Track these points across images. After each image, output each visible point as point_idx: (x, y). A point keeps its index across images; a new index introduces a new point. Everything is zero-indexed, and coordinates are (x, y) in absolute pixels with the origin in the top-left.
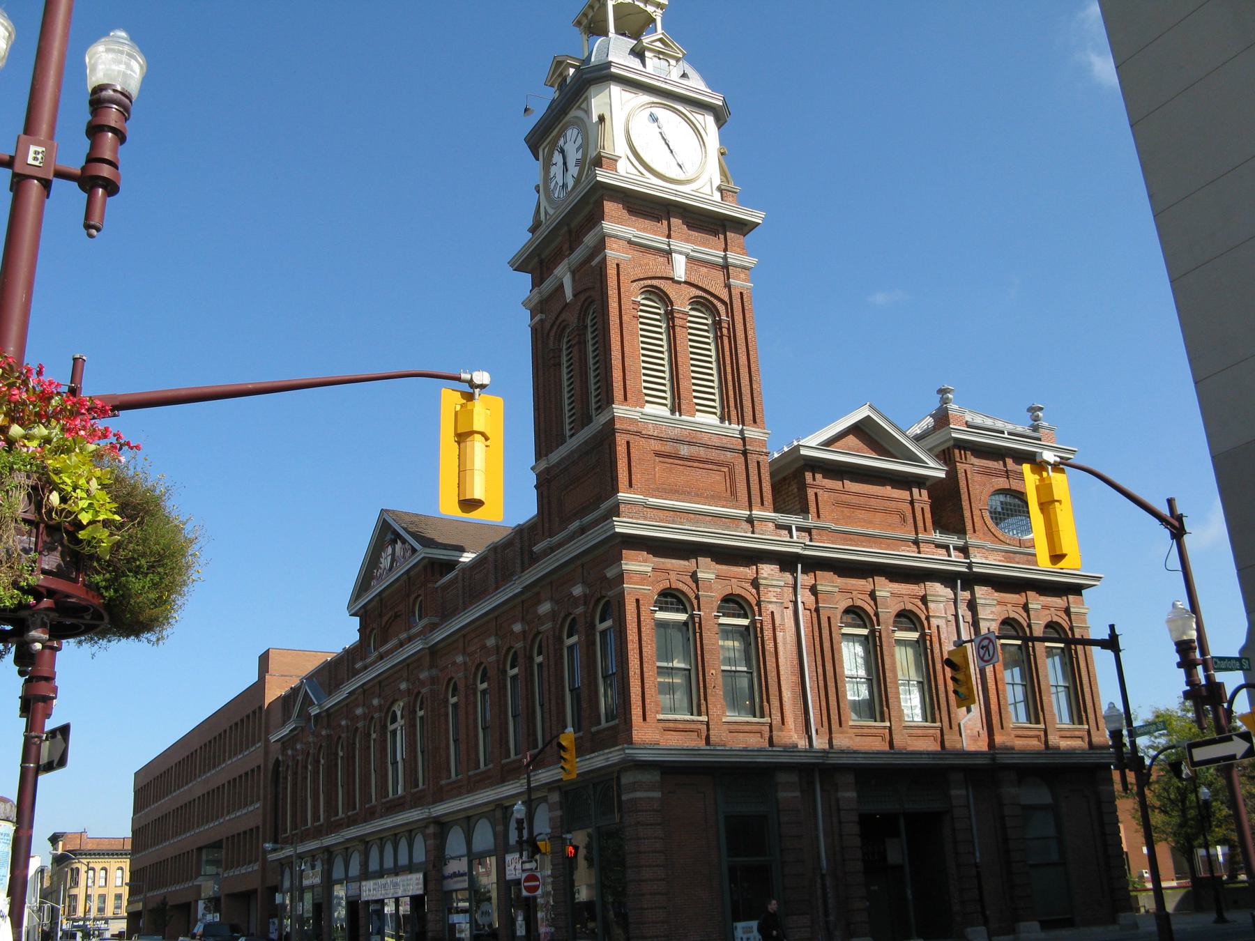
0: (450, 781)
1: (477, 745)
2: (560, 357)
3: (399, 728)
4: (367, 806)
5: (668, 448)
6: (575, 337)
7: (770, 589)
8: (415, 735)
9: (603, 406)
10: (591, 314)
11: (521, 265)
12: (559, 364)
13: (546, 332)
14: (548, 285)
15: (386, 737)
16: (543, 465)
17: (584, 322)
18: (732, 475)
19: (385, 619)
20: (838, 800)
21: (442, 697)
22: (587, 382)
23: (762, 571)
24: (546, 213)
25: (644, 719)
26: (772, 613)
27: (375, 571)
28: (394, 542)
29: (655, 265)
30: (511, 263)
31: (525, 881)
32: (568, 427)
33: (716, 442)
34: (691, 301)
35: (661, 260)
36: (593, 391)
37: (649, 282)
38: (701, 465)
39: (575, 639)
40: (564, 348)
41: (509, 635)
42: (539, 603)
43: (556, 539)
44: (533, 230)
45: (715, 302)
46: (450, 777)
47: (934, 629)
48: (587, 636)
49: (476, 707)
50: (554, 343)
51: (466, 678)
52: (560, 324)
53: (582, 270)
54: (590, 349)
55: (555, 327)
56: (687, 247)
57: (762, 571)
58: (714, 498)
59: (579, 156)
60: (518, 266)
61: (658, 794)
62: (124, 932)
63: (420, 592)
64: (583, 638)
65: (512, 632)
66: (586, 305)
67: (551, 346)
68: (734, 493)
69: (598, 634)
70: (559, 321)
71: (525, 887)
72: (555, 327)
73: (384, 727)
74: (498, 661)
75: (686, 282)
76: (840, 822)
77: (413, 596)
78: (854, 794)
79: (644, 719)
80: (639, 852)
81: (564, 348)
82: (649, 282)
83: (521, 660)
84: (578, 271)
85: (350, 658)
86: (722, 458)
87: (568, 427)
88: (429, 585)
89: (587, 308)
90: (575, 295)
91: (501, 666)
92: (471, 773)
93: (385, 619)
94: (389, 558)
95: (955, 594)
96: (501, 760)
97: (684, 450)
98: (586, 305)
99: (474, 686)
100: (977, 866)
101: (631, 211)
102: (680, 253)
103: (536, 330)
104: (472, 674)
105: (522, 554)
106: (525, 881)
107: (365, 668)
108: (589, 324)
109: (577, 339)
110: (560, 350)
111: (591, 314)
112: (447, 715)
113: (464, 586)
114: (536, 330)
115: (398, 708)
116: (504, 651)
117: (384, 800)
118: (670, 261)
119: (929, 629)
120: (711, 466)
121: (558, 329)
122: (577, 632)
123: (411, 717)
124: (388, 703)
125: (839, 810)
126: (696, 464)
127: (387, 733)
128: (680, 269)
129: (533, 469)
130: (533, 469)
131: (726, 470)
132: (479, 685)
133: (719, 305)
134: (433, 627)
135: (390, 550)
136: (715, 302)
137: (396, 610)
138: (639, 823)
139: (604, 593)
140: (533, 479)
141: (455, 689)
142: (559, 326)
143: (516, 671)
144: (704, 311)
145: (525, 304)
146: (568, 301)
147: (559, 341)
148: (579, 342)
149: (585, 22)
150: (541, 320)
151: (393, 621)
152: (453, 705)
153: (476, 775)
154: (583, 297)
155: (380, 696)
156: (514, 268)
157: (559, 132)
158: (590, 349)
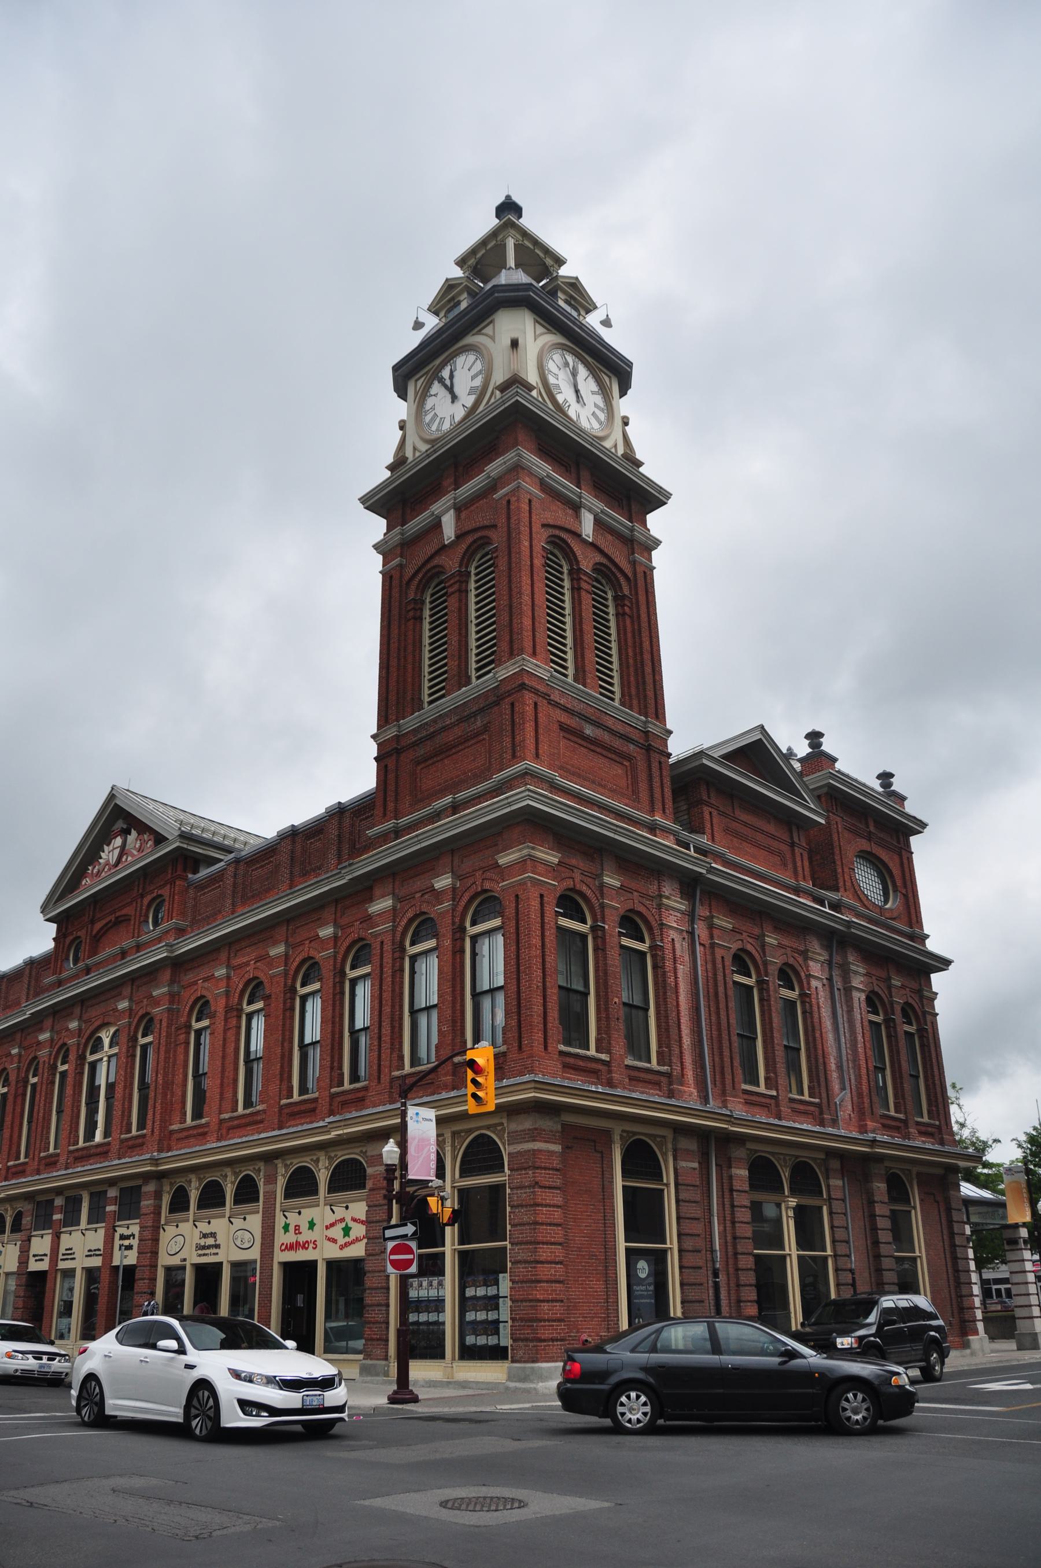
0: (235, 1114)
1: (235, 1081)
2: (421, 610)
3: (105, 1059)
4: (42, 1154)
5: (572, 722)
6: (455, 583)
7: (671, 912)
8: (133, 1068)
9: (500, 660)
10: (476, 560)
11: (376, 502)
12: (420, 619)
13: (406, 578)
14: (417, 523)
15: (83, 1069)
16: (391, 732)
17: (467, 567)
18: (634, 768)
19: (98, 926)
20: (731, 1177)
21: (183, 1020)
22: (466, 636)
23: (664, 889)
24: (415, 449)
25: (546, 1048)
26: (673, 940)
27: (90, 868)
28: (126, 832)
29: (561, 516)
30: (364, 500)
31: (392, 1253)
32: (426, 692)
33: (619, 728)
34: (598, 567)
35: (570, 512)
36: (426, 674)
37: (557, 532)
38: (604, 753)
39: (149, 1039)
40: (428, 600)
41: (308, 942)
42: (41, 1030)
43: (404, 821)
44: (391, 468)
45: (619, 575)
46: (185, 1121)
47: (813, 990)
48: (454, 940)
49: (24, 1100)
50: (416, 593)
51: (227, 994)
52: (429, 570)
54: (472, 599)
55: (420, 575)
56: (599, 505)
57: (664, 889)
58: (614, 793)
59: (478, 382)
60: (372, 504)
61: (557, 1148)
62: (255, 1261)
63: (79, 934)
64: (124, 1050)
65: (67, 1029)
66: (473, 548)
67: (411, 596)
68: (635, 792)
69: (139, 1049)
70: (429, 566)
71: (393, 1262)
72: (420, 575)
73: (82, 1058)
74: (286, 973)
75: (592, 544)
76: (733, 1206)
77: (146, 901)
78: (747, 1173)
79: (546, 1048)
80: (536, 1223)
81: (428, 600)
82: (557, 532)
83: (72, 1057)
84: (466, 508)
85: (34, 973)
86: (625, 749)
87: (426, 692)
88: (177, 883)
89: (432, 578)
90: (459, 537)
91: (290, 982)
92: (11, 1163)
93: (98, 926)
94: (117, 852)
95: (831, 956)
96: (280, 1099)
97: (589, 730)
98: (473, 548)
99: (239, 1007)
100: (851, 1271)
101: (542, 451)
102: (590, 510)
103: (391, 577)
104: (238, 991)
105: (340, 842)
106: (392, 1253)
107: (60, 983)
108: (473, 572)
109: (456, 587)
110: (423, 602)
111: (476, 560)
112: (188, 1043)
113: (235, 884)
114: (391, 577)
115: (106, 1037)
116: (295, 964)
117: (72, 1148)
118: (577, 516)
119: (809, 989)
120: (613, 756)
121: (423, 577)
122: (117, 1044)
123: (130, 1044)
124: (92, 1028)
125: (731, 1190)
126: (599, 750)
127: (84, 1065)
128: (587, 527)
129: (374, 737)
130: (374, 737)
131: (626, 763)
132: (31, 1079)
133: (622, 580)
134: (180, 932)
135: (118, 841)
136: (619, 575)
137: (118, 914)
138: (537, 1183)
139: (149, 1009)
140: (373, 749)
141: (36, 1070)
142: (426, 573)
143: (65, 1067)
144: (604, 581)
145: (376, 547)
146: (446, 543)
147: (423, 592)
148: (460, 591)
149: (472, 262)
150: (401, 566)
151: (111, 927)
152: (61, 1073)
153: (15, 1166)
155: (81, 1017)
156: (366, 505)
157: (441, 363)
158: (472, 599)
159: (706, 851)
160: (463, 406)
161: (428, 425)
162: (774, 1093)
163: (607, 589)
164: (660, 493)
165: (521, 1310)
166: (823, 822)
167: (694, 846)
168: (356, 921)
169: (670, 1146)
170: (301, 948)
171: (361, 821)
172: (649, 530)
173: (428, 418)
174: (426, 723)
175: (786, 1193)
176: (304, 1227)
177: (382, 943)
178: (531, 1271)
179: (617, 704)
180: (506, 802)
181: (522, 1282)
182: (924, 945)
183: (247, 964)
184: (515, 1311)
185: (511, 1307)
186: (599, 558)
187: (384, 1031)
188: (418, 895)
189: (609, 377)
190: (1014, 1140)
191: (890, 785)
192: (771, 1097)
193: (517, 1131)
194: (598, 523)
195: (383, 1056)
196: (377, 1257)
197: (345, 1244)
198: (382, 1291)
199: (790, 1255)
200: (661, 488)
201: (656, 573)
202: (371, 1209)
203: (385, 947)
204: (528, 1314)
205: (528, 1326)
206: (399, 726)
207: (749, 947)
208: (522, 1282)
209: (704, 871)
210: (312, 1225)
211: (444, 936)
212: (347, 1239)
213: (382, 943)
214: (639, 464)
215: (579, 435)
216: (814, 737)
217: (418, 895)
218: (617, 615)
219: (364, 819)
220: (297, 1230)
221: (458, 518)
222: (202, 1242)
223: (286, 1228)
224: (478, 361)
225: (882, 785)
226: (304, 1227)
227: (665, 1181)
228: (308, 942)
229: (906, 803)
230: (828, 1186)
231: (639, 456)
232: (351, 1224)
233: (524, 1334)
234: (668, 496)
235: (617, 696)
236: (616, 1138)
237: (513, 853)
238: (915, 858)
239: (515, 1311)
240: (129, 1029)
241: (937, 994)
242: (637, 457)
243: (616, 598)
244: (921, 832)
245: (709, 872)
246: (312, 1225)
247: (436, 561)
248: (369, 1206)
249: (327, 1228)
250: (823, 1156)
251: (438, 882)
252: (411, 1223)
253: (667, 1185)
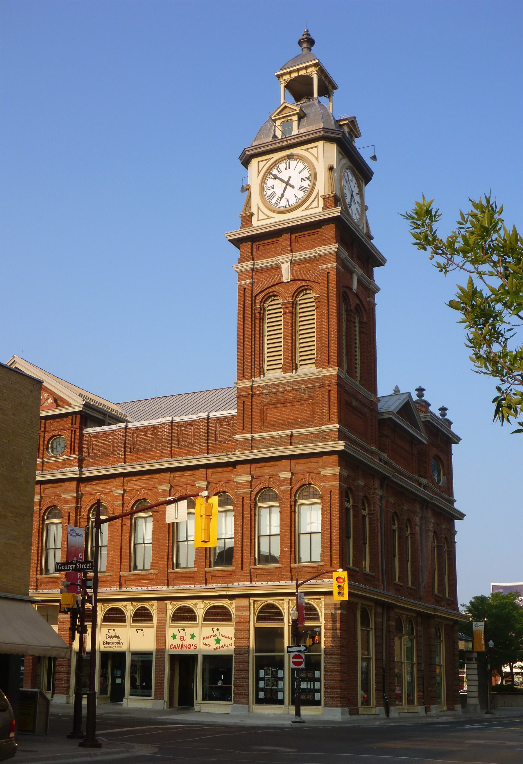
41: (185, 486)
45: (363, 310)
53: (302, 266)
131: (364, 418)
136: (363, 310)
154: (300, 284)
159: (386, 462)
160: (295, 196)
161: (269, 197)
162: (402, 584)
163: (356, 317)
164: (374, 250)
165: (330, 684)
166: (426, 442)
167: (384, 460)
168: (221, 481)
169: (373, 611)
170: (180, 488)
171: (221, 425)
172: (374, 281)
173: (269, 192)
174: (271, 385)
175: (404, 633)
176: (188, 637)
177: (243, 498)
178: (336, 667)
179: (358, 383)
180: (331, 445)
181: (331, 672)
182: (453, 505)
183: (138, 490)
184: (327, 684)
185: (325, 683)
186: (358, 302)
187: (245, 544)
188: (267, 478)
189: (362, 181)
190: (201, 516)
191: (445, 415)
192: (401, 586)
193: (330, 604)
194: (359, 282)
195: (245, 557)
196: (242, 656)
197: (217, 648)
198: (246, 672)
199: (372, 658)
200: (384, 257)
201: (377, 307)
202: (237, 632)
203: (245, 501)
204: (335, 686)
205: (334, 691)
206: (253, 381)
207: (397, 511)
208: (331, 672)
209: (391, 476)
210: (193, 637)
211: (285, 502)
212: (218, 645)
213: (243, 498)
214: (371, 238)
215: (350, 223)
216: (420, 390)
217: (267, 478)
218: (360, 332)
219: (223, 425)
220: (182, 638)
221: (292, 269)
222: (109, 640)
223: (174, 637)
224: (306, 170)
225: (441, 415)
226: (188, 637)
227: (371, 627)
228: (185, 486)
229: (452, 426)
230: (417, 630)
231: (372, 233)
232: (220, 638)
233: (332, 695)
234: (385, 261)
235: (358, 379)
236: (359, 607)
237: (330, 470)
238: (453, 457)
239: (327, 684)
240: (40, 512)
241: (457, 532)
242: (371, 234)
243: (360, 323)
244: (457, 443)
245: (393, 476)
246: (193, 637)
247: (275, 289)
248: (235, 630)
249: (204, 639)
250: (415, 615)
251: (282, 474)
252: (303, 645)
253: (372, 629)
